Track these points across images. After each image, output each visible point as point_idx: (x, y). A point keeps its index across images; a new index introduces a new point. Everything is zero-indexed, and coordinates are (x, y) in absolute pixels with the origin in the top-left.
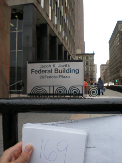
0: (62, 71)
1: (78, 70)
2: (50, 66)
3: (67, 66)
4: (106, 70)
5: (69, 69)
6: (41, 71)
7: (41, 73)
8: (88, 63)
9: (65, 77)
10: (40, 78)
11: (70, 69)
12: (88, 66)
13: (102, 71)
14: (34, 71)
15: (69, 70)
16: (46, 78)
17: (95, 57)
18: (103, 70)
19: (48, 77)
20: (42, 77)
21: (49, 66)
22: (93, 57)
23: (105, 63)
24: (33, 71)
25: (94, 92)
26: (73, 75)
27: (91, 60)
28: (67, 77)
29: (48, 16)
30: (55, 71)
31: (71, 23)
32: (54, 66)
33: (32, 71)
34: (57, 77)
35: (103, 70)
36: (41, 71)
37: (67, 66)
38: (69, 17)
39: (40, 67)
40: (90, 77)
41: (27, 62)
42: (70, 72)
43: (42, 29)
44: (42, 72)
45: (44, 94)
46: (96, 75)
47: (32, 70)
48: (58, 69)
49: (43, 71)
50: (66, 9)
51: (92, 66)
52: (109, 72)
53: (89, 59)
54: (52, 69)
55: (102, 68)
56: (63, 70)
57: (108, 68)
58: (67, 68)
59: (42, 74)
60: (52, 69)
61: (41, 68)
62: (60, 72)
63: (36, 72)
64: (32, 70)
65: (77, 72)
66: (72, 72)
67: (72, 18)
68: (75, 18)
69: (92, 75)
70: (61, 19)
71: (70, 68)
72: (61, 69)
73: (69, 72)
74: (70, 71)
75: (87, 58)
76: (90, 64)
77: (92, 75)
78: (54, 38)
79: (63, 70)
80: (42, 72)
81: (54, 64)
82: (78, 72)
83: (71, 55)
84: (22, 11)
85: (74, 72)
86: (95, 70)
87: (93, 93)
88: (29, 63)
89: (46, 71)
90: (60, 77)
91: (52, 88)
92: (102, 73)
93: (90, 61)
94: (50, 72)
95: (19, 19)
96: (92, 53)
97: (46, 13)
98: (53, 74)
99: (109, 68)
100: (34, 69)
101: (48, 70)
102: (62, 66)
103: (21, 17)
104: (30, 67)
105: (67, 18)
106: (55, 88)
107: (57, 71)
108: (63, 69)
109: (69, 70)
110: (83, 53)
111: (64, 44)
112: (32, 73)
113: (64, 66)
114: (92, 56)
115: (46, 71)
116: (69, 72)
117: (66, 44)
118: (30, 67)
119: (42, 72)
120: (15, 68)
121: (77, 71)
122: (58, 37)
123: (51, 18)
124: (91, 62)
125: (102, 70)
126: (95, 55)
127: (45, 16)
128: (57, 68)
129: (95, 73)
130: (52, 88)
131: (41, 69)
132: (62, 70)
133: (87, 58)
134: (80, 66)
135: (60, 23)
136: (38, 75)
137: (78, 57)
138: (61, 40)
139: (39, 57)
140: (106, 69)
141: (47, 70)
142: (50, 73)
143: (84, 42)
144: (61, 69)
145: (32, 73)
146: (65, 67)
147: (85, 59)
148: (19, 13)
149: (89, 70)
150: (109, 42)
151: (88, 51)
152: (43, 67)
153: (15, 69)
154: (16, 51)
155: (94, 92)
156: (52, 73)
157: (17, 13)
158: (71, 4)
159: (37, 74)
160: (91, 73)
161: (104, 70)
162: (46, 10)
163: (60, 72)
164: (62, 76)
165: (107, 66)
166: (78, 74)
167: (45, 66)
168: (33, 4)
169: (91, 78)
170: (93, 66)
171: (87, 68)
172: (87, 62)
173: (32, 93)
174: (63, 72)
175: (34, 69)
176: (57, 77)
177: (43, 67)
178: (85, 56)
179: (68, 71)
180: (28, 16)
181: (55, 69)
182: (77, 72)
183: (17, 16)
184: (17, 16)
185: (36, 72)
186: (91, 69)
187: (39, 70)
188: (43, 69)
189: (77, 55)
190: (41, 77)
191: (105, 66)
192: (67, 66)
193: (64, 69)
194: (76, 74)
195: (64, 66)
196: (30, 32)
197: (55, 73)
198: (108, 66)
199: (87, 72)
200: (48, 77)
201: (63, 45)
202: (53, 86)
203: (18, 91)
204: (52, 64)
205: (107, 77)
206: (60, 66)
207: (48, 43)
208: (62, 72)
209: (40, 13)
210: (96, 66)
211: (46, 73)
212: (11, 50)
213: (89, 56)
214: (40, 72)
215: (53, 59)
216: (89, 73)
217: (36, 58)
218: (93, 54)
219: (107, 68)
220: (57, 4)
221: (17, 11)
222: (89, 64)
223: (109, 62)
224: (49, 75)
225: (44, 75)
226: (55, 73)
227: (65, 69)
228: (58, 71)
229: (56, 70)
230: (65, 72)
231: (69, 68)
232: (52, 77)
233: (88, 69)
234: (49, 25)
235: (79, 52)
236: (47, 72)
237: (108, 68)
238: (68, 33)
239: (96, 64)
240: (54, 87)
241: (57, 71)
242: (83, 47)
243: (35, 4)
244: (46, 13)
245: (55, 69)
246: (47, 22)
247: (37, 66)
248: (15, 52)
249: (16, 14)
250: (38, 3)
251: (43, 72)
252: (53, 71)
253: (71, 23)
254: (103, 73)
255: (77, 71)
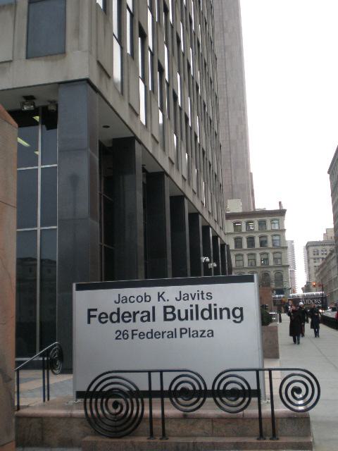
0: (189, 315)
1: (241, 309)
2: (148, 299)
3: (205, 296)
4: (326, 261)
5: (210, 305)
6: (121, 315)
7: (118, 321)
8: (266, 242)
9: (200, 333)
10: (117, 338)
11: (213, 307)
12: (267, 251)
13: (312, 264)
14: (97, 313)
15: (210, 310)
16: (136, 337)
17: (288, 222)
18: (314, 259)
19: (141, 335)
20: (122, 335)
21: (146, 298)
22: (281, 223)
23: (321, 239)
24: (95, 316)
25: (298, 390)
26: (223, 326)
27: (276, 230)
28: (205, 334)
29: (137, 115)
30: (165, 313)
31: (208, 123)
32: (160, 296)
33: (90, 316)
34: (172, 335)
35: (314, 259)
36: (118, 314)
37: (203, 299)
38: (201, 108)
39: (117, 301)
40: (273, 286)
41: (74, 285)
42: (216, 318)
43: (117, 154)
44: (123, 317)
45: (131, 391)
46: (293, 278)
47: (89, 310)
48: (173, 308)
49: (127, 315)
50: (189, 82)
51: (280, 250)
52: (335, 267)
53: (269, 228)
54: (154, 308)
55: (311, 255)
56: (192, 311)
57: (332, 252)
58: (203, 304)
59: (122, 326)
60: (154, 308)
61: (118, 305)
62: (183, 316)
63: (104, 318)
64: (89, 310)
65: (237, 315)
66: (221, 317)
67: (209, 110)
68: (221, 102)
69: (280, 279)
70: (177, 117)
71: (215, 305)
72: (182, 306)
73: (210, 317)
74: (214, 313)
75: (262, 224)
76: (273, 245)
77: (282, 276)
78: (156, 179)
79: (192, 311)
80: (123, 317)
81: (160, 289)
82: (242, 316)
83: (212, 224)
84: (55, 103)
85: (229, 317)
86: (290, 262)
87: (295, 394)
88: (80, 288)
89: (135, 314)
90: (181, 333)
91: (156, 376)
92: (313, 271)
93: (272, 236)
94: (149, 316)
95: (44, 126)
96: (277, 208)
97: (130, 105)
98: (159, 325)
99: (334, 255)
100: (96, 310)
101: (142, 313)
102: (186, 297)
103: (50, 119)
104: (83, 300)
105: (196, 112)
106: (168, 378)
107: (170, 313)
108: (191, 306)
109: (210, 310)
110: (248, 211)
111: (189, 194)
112: (89, 322)
113: (193, 299)
114: (277, 218)
115: (135, 314)
116: (210, 317)
117: (193, 191)
118: (83, 300)
119: (121, 317)
120: (36, 260)
121: (238, 313)
122: (168, 175)
123: (142, 114)
124: (277, 238)
125: (312, 261)
126: (287, 214)
127: (125, 114)
128: (172, 302)
129: (289, 253)
130: (156, 376)
131: (118, 309)
132: (186, 311)
133: (262, 224)
134: (245, 295)
135: (173, 131)
136: (111, 328)
137: (234, 224)
138: (179, 182)
139: (113, 272)
140: (325, 256)
141: (138, 312)
142: (149, 320)
143: (251, 174)
144: (182, 306)
145: (89, 322)
146: (195, 302)
147: (257, 228)
148: (45, 108)
149: (271, 263)
150: (329, 173)
151: (263, 202)
152: (126, 300)
153: (36, 265)
154: (39, 229)
155: (298, 390)
156: (154, 320)
157: (35, 112)
158: (210, 165)
159: (105, 324)
160: (278, 272)
161: (318, 259)
162: (129, 96)
163: (183, 316)
164: (187, 331)
165: (328, 248)
166: (240, 322)
167: (132, 299)
168: (88, 81)
169: (279, 287)
170: (282, 248)
171: (265, 256)
172: (263, 239)
173: (92, 389)
174: (192, 319)
175: (96, 310)
176: (172, 335)
177: (126, 300)
178: (256, 220)
179: (206, 314)
180: (73, 114)
181: (165, 308)
182: (237, 315)
183: (37, 118)
184: (37, 118)
185: (104, 318)
186: (275, 259)
187: (111, 312)
188: (124, 308)
189: (229, 216)
190: (121, 337)
191: (320, 248)
192: (203, 299)
193: (194, 308)
194: (235, 321)
195: (193, 299)
196: (84, 166)
197: (166, 319)
198: (333, 247)
199: (265, 269)
200: (141, 335)
201: (187, 198)
202: (161, 372)
203: (43, 360)
204: (153, 291)
205: (330, 281)
206: (182, 297)
207: (140, 196)
208: (186, 318)
209: (112, 107)
210: (293, 247)
211: (134, 321)
212: (18, 227)
213: (268, 219)
214: (115, 317)
215: (156, 274)
216: (272, 274)
217: (100, 195)
218: (281, 213)
219: (329, 252)
220: (161, 70)
221: (38, 103)
222: (270, 244)
223: (332, 234)
224: (146, 327)
225: (130, 326)
226: (166, 319)
227: (197, 306)
228: (176, 312)
229: (169, 310)
230: (197, 318)
231: (212, 302)
232: (154, 335)
233: (266, 260)
234: (140, 143)
235: (235, 206)
236: (138, 316)
237: (331, 254)
238: (200, 156)
239: (292, 242)
240: (164, 373)
241: (172, 313)
242: (247, 191)
243: (95, 81)
244: (130, 105)
245: (165, 308)
246: (134, 133)
247: (106, 299)
248: (37, 169)
249: (35, 112)
250: (104, 77)
251: (126, 319)
252: (159, 314)
253: (208, 123)
254: (317, 271)
255: (238, 313)
